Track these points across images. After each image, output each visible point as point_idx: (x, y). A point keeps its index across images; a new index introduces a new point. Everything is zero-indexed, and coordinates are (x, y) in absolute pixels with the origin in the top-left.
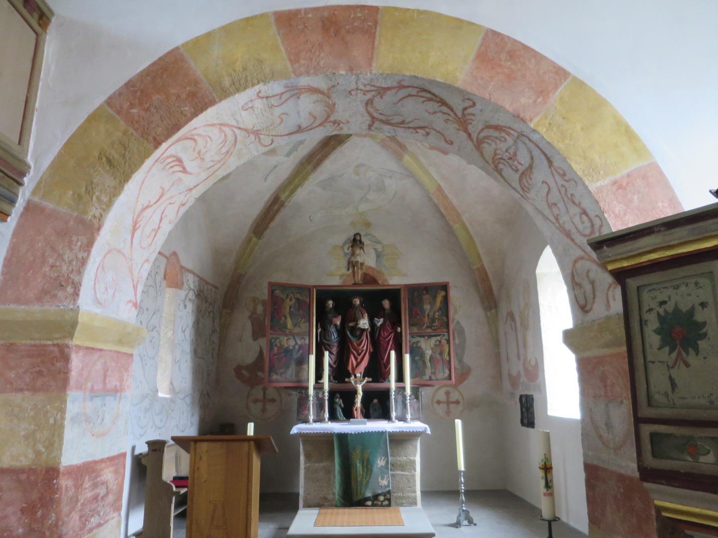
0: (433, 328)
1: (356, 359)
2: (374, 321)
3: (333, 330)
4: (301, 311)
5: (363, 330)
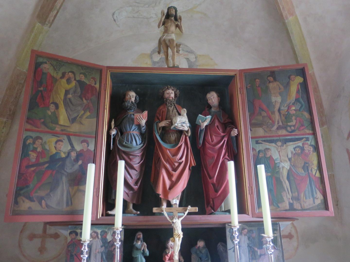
0: (289, 128)
1: (170, 176)
2: (198, 118)
3: (134, 132)
4: (85, 101)
5: (181, 132)
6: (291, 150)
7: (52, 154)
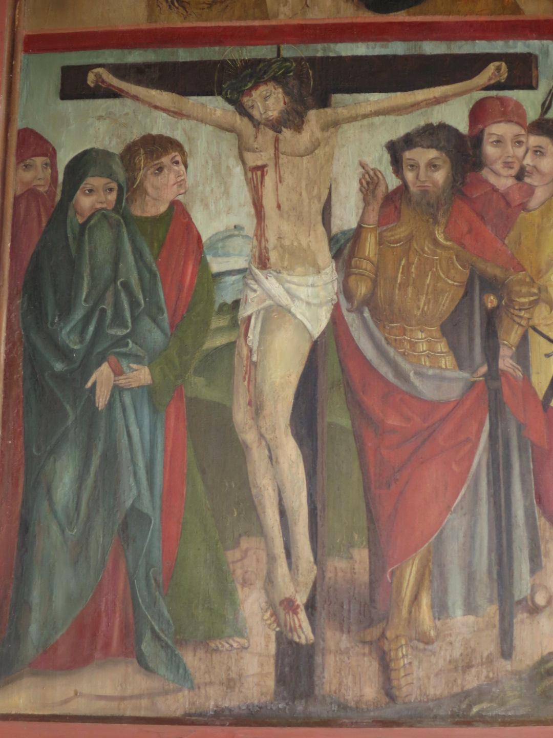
6: (363, 165)
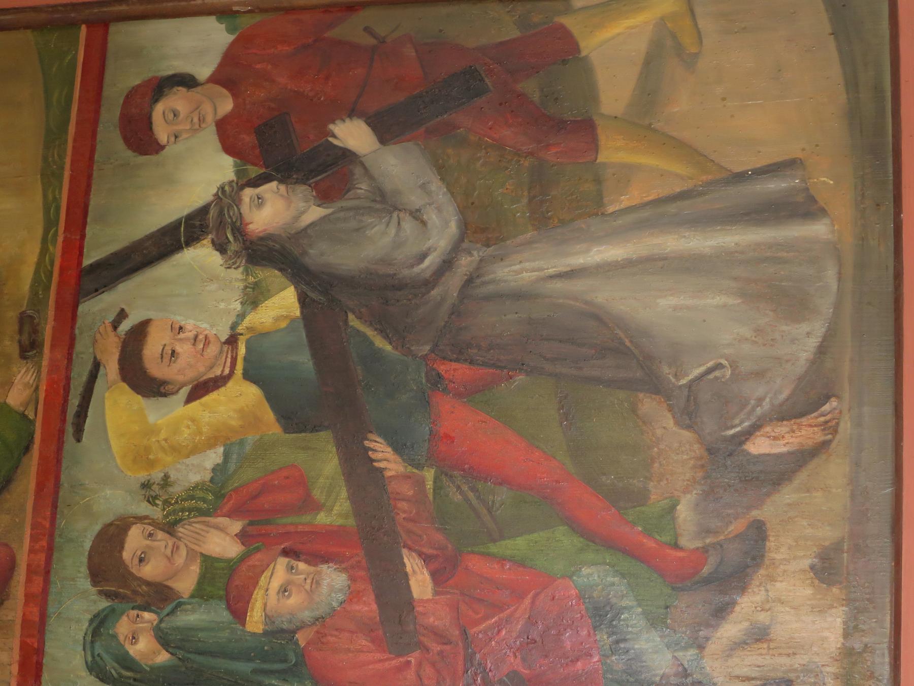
7: (269, 415)
